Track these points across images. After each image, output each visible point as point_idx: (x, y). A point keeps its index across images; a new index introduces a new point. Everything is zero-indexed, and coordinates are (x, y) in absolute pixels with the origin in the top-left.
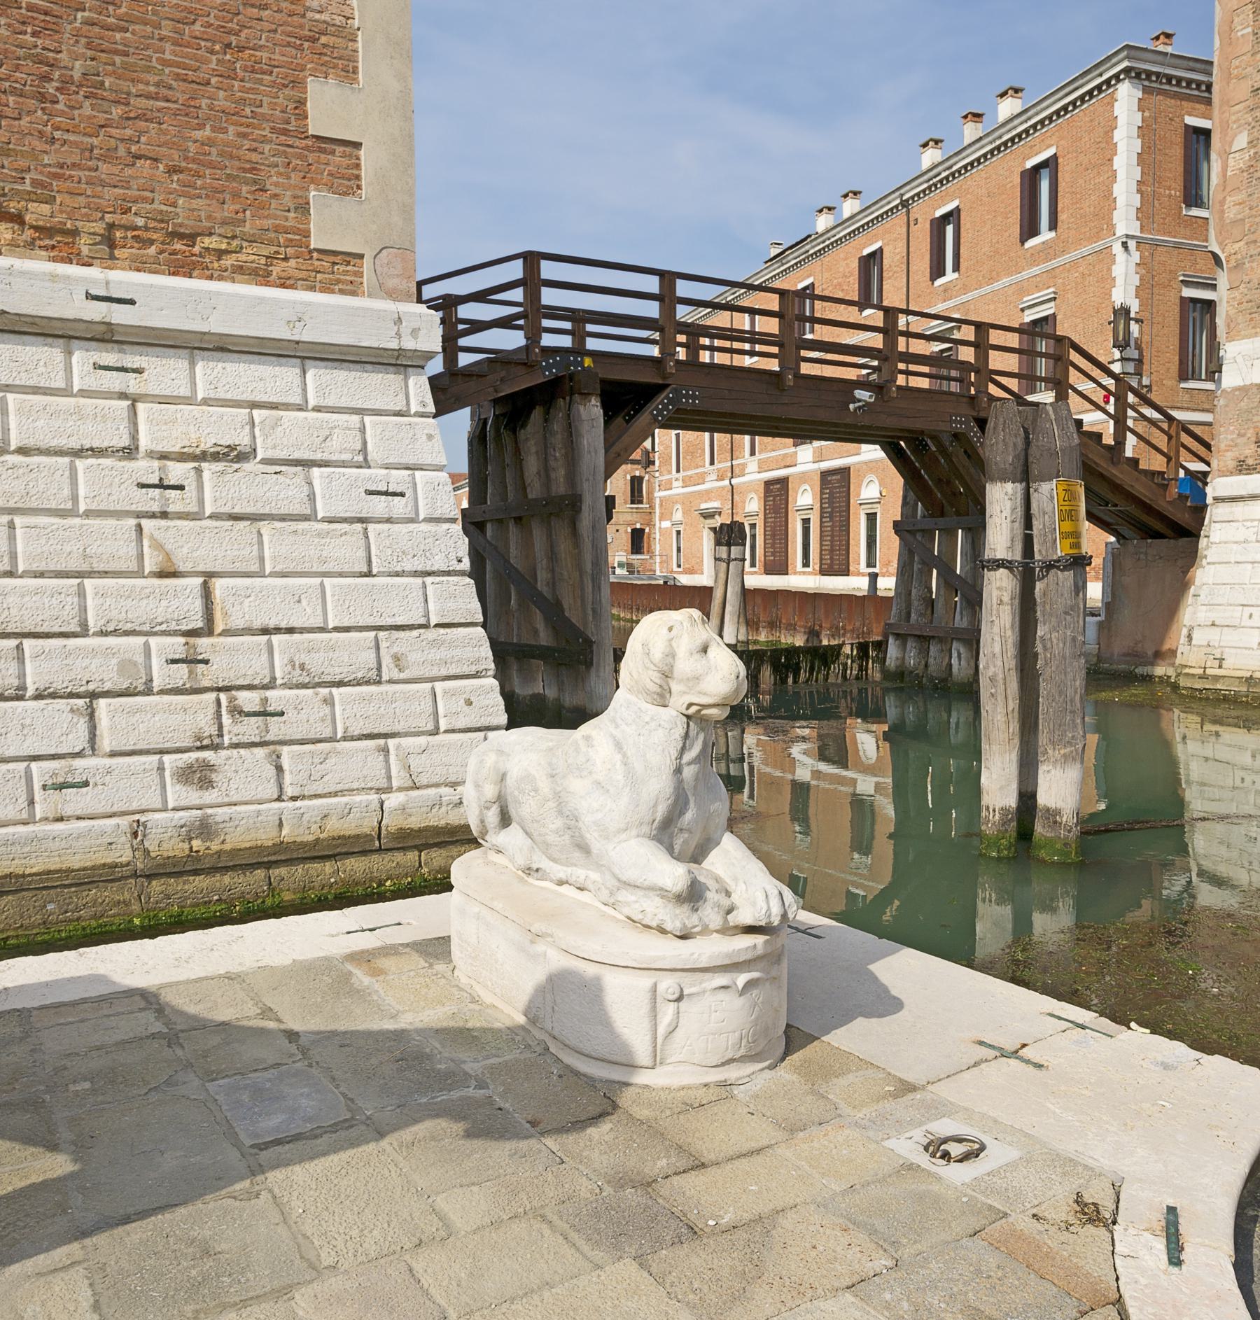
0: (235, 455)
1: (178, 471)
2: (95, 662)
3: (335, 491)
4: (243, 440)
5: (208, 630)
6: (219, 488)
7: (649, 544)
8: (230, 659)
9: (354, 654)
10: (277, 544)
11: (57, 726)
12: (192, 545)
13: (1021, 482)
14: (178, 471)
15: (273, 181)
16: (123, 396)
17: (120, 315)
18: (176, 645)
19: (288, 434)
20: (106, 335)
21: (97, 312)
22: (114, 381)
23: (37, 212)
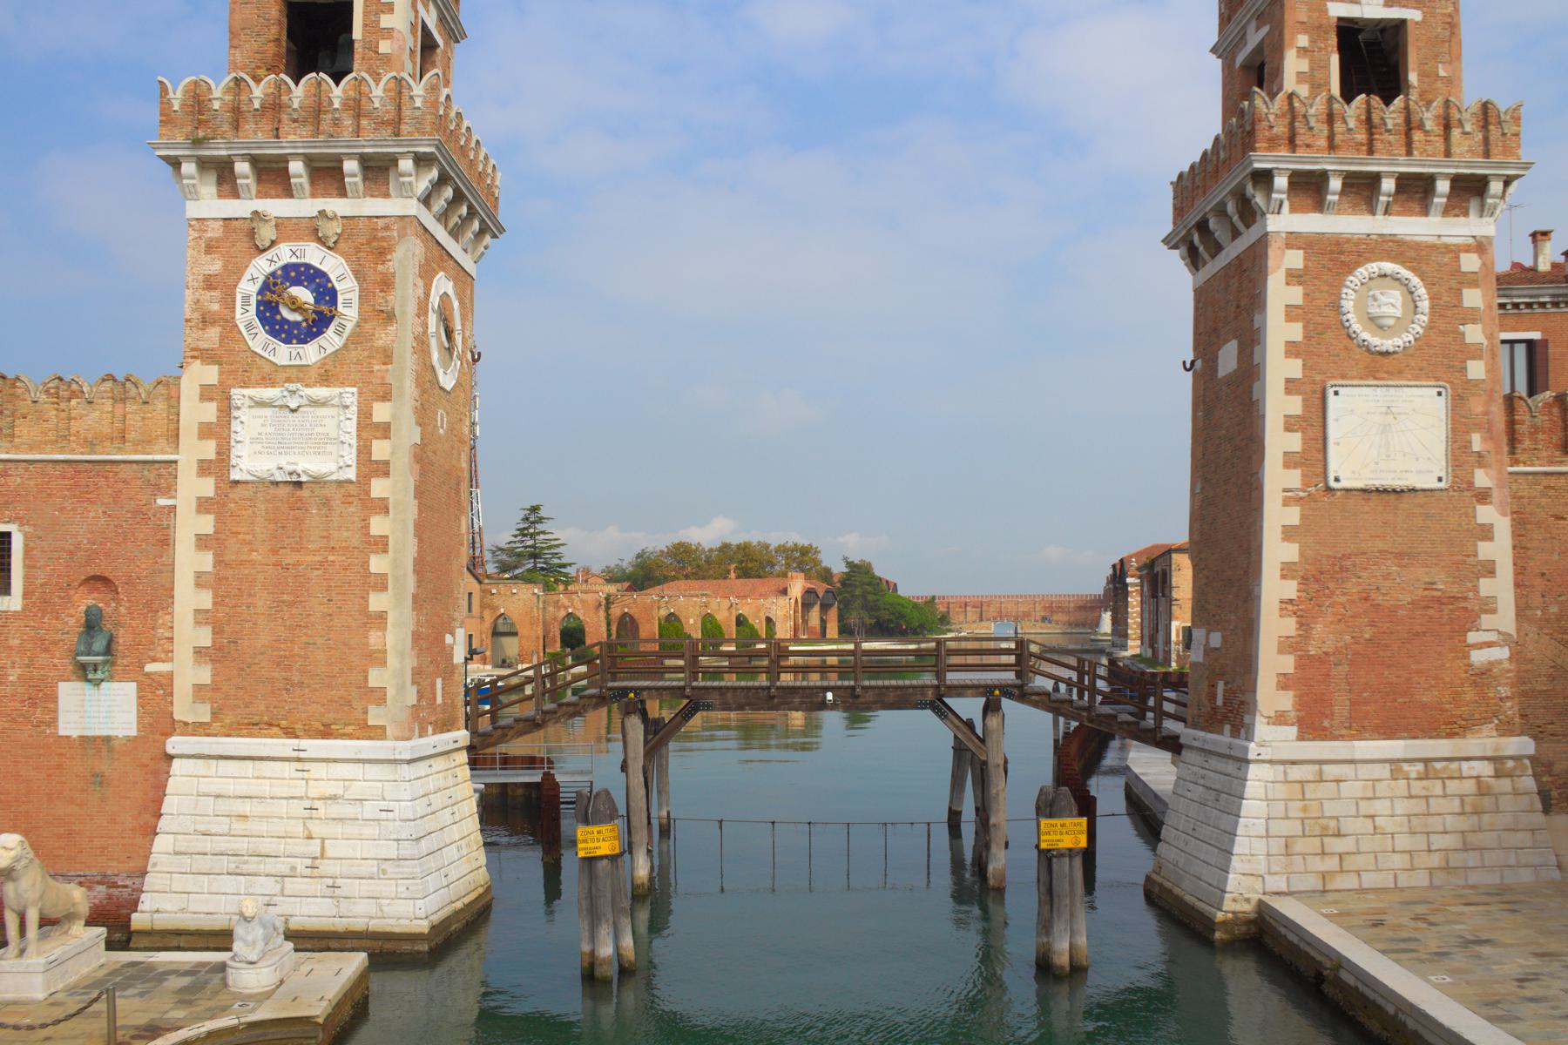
0: (334, 798)
1: (317, 804)
2: (282, 866)
3: (370, 810)
4: (340, 792)
5: (322, 856)
6: (335, 810)
7: (1322, 954)
8: (326, 867)
9: (372, 867)
10: (350, 829)
11: (270, 886)
12: (317, 829)
13: (1081, 814)
14: (317, 804)
15: (355, 704)
16: (1402, 889)
17: (302, 755)
18: (309, 862)
19: (356, 790)
20: (299, 760)
21: (295, 754)
22: (300, 774)
23: (284, 723)
